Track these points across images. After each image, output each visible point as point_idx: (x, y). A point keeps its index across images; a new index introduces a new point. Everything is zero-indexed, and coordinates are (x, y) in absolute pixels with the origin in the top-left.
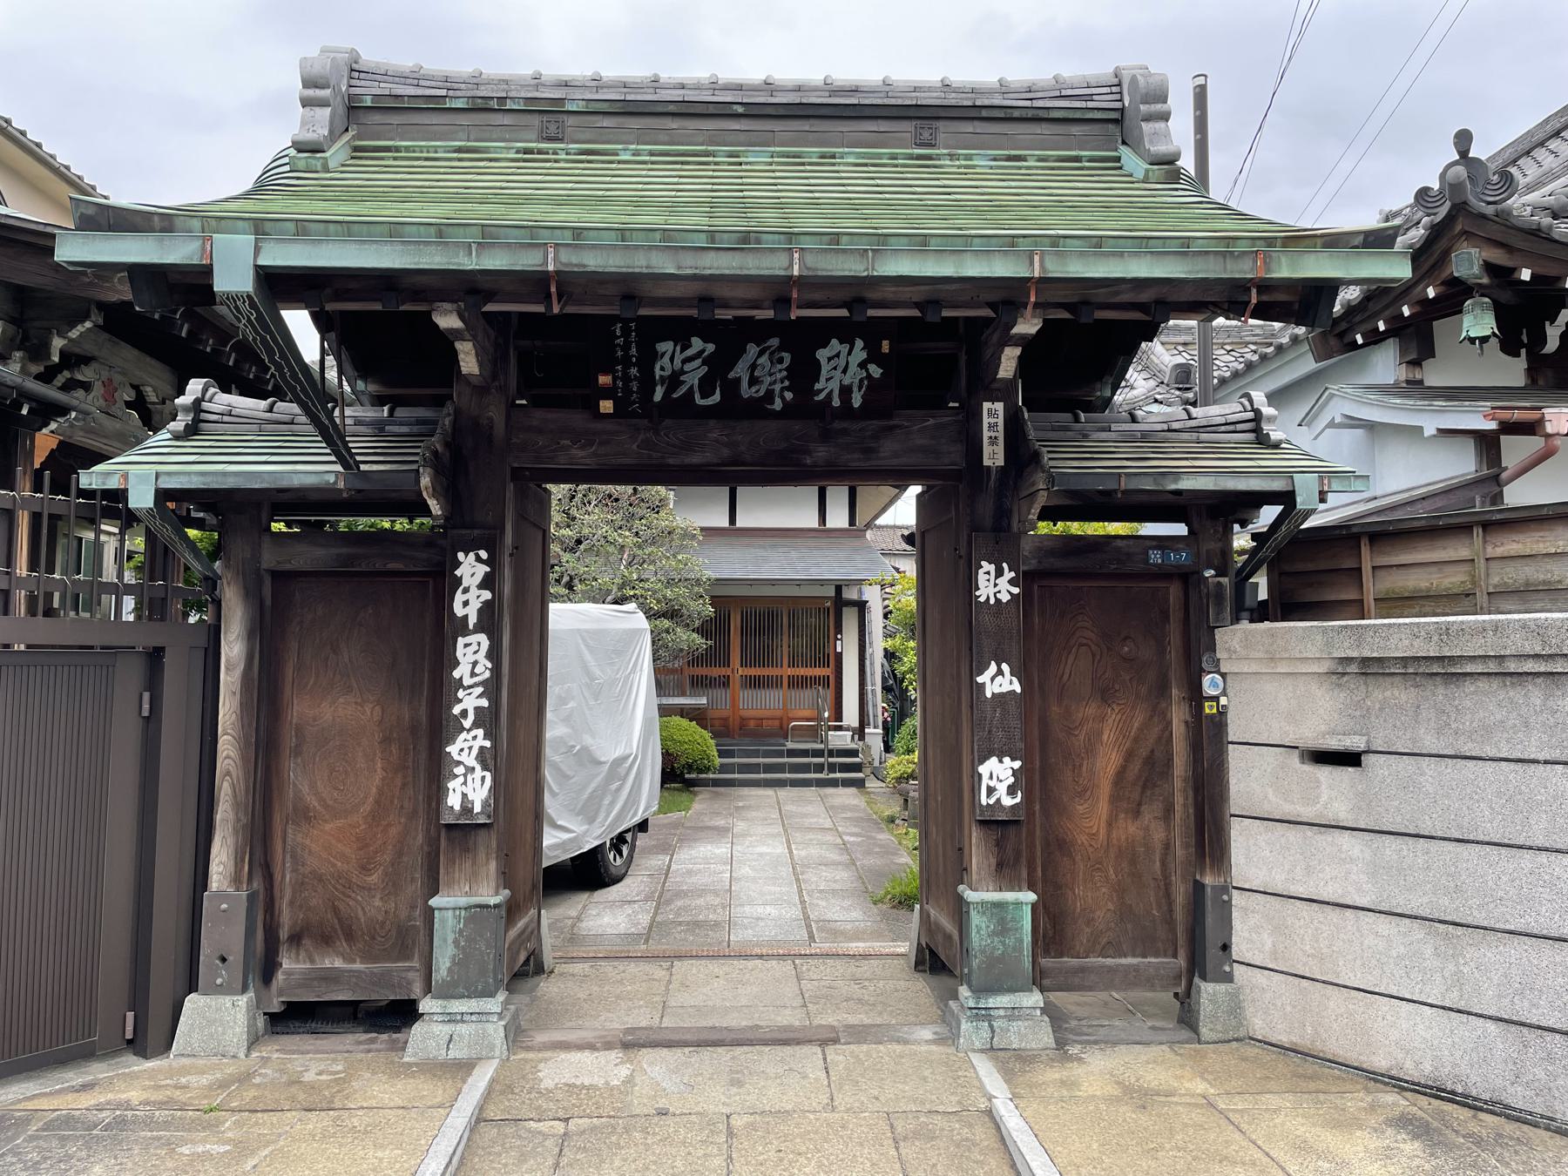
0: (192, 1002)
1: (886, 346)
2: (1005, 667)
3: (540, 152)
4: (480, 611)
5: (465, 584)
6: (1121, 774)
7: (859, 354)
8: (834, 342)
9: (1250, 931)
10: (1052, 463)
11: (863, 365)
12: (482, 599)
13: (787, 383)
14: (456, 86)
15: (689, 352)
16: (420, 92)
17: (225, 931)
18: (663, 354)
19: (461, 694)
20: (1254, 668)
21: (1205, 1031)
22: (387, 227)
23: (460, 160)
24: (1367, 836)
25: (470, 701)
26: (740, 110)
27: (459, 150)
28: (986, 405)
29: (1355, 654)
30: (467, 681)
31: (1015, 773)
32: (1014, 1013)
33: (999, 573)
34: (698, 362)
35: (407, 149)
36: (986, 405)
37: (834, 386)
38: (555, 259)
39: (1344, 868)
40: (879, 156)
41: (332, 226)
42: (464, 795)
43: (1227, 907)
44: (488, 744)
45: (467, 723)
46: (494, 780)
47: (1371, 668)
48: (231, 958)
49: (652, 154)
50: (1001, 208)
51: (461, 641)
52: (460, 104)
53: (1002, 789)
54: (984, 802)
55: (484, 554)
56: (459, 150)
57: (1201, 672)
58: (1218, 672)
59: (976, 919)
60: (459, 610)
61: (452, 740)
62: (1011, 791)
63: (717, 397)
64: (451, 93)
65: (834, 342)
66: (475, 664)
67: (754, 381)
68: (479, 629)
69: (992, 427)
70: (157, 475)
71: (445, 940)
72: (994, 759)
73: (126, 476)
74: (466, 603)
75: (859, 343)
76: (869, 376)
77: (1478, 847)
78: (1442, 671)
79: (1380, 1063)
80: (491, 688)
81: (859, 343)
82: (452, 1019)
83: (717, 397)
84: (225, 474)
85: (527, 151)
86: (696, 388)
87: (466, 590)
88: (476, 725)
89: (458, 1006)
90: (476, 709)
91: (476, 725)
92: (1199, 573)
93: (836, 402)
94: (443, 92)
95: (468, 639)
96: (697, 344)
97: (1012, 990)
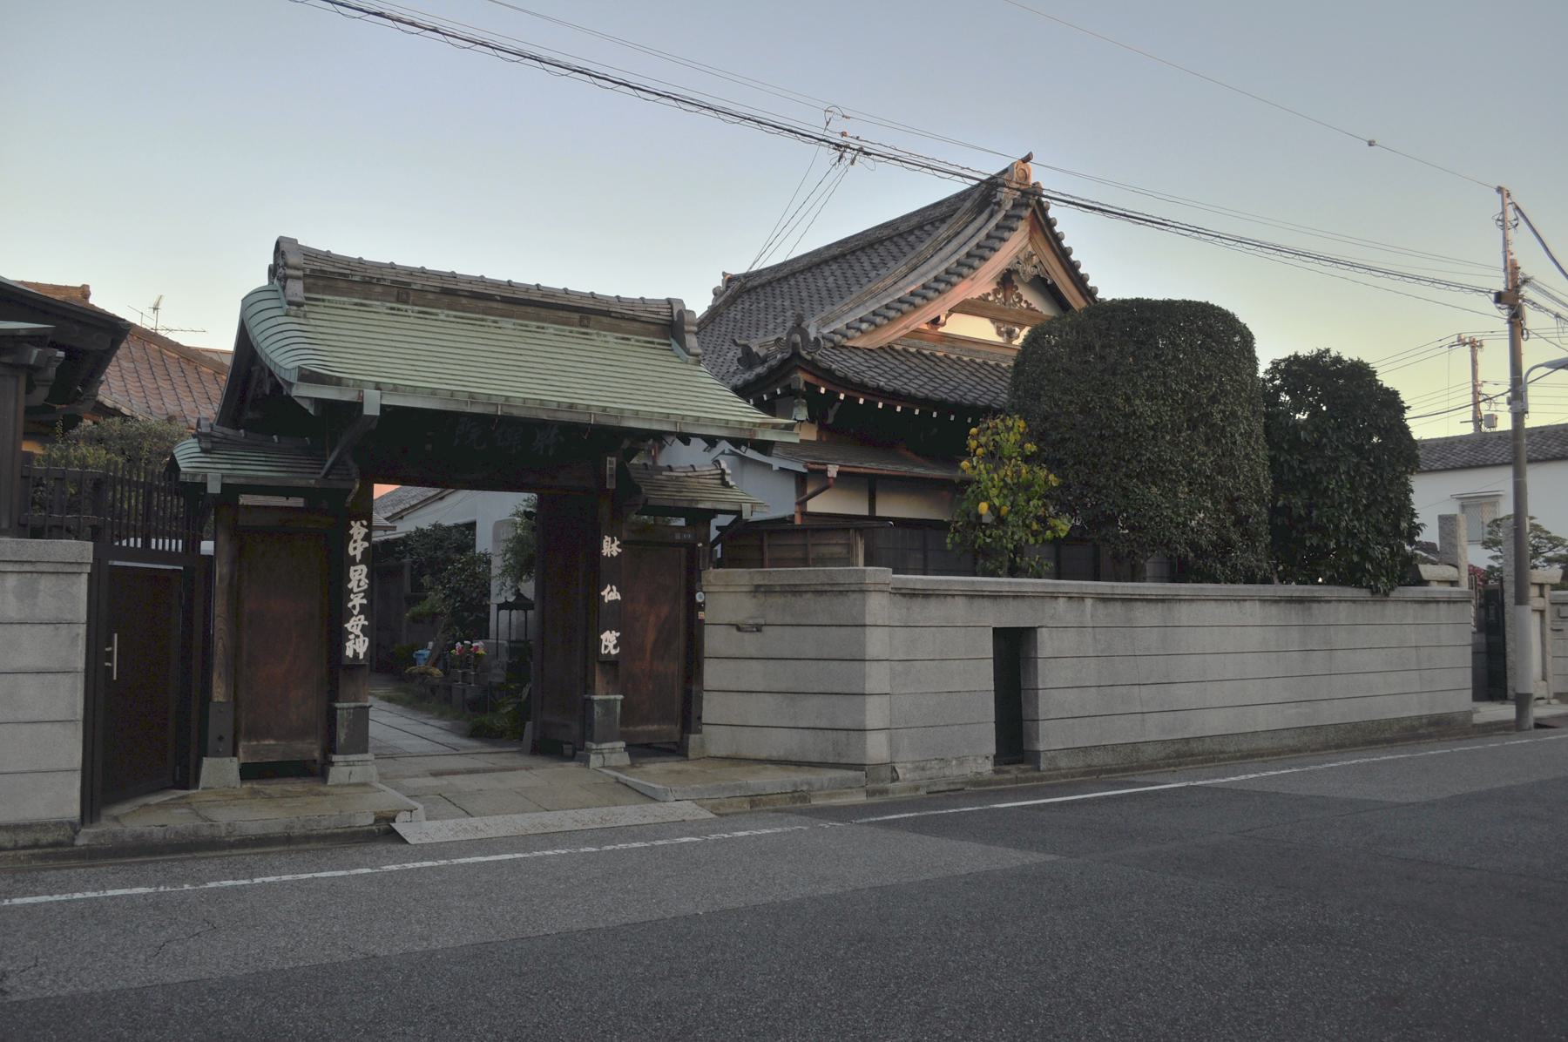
0: (206, 761)
9: (712, 708)
17: (219, 724)
21: (691, 755)
25: (357, 601)
32: (613, 750)
39: (753, 676)
43: (700, 699)
53: (611, 646)
59: (597, 709)
60: (351, 552)
62: (615, 647)
68: (361, 562)
73: (205, 476)
78: (795, 591)
79: (763, 755)
80: (368, 594)
82: (348, 764)
89: (352, 757)
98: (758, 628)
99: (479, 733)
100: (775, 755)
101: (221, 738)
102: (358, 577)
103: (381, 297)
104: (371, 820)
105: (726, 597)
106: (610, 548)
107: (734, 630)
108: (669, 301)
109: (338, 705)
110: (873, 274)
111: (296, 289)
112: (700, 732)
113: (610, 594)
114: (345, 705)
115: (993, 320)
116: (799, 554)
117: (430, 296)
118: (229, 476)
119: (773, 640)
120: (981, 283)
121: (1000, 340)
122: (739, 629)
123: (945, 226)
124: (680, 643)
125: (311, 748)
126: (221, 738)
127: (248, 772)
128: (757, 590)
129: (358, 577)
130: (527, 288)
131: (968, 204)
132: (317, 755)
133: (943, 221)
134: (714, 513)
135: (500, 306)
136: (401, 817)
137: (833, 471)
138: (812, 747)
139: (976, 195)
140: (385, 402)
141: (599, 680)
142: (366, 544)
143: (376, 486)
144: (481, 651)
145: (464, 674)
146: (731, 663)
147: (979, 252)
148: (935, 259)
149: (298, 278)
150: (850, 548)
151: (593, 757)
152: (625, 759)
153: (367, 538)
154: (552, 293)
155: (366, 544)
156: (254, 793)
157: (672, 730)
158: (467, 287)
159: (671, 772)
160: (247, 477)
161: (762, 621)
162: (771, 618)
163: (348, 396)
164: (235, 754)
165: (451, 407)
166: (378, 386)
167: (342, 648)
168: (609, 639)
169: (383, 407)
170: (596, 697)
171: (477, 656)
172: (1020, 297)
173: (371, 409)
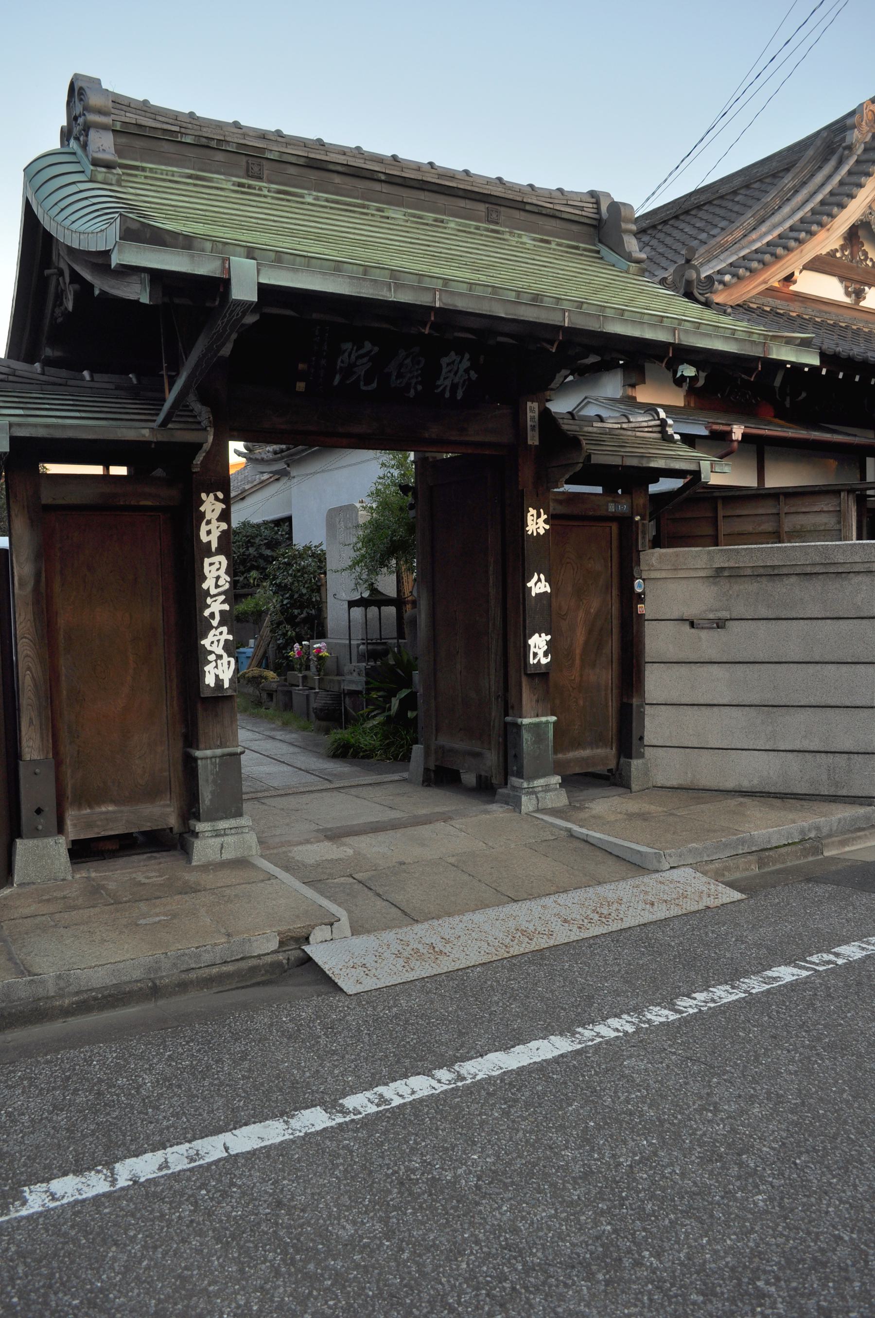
0: (20, 845)
1: (482, 359)
2: (542, 577)
3: (250, 187)
4: (219, 538)
5: (208, 517)
6: (586, 643)
7: (466, 364)
8: (453, 353)
9: (655, 726)
10: (589, 447)
11: (467, 371)
12: (221, 529)
13: (420, 379)
14: (184, 125)
15: (361, 352)
16: (159, 125)
17: (35, 790)
18: (344, 351)
19: (209, 601)
20: (663, 575)
21: (634, 787)
22: (333, 264)
23: (195, 185)
24: (727, 666)
25: (216, 606)
26: (383, 177)
27: (190, 177)
28: (529, 404)
29: (726, 565)
30: (213, 591)
31: (548, 643)
32: (547, 789)
33: (539, 516)
34: (365, 360)
35: (151, 170)
36: (529, 404)
37: (448, 383)
38: (440, 299)
39: (715, 683)
40: (469, 226)
41: (298, 258)
42: (217, 676)
43: (642, 716)
44: (231, 637)
45: (215, 623)
46: (237, 662)
47: (732, 574)
48: (46, 809)
49: (327, 200)
50: (447, 260)
51: (207, 561)
52: (189, 140)
53: (541, 653)
54: (531, 662)
55: (220, 495)
56: (190, 177)
57: (633, 579)
58: (641, 578)
59: (526, 736)
60: (204, 538)
61: (205, 636)
62: (546, 654)
63: (375, 385)
64: (183, 130)
65: (453, 353)
66: (218, 578)
67: (400, 376)
68: (219, 551)
69: (532, 418)
70: (11, 425)
71: (207, 780)
72: (537, 635)
74: (209, 532)
75: (467, 356)
76: (469, 379)
77: (787, 665)
78: (774, 574)
79: (730, 785)
81: (467, 356)
82: (217, 834)
83: (375, 385)
84: (64, 426)
85: (240, 185)
86: (362, 378)
87: (209, 522)
88: (221, 624)
89: (222, 825)
90: (221, 612)
91: (221, 624)
92: (632, 518)
93: (447, 395)
94: (177, 129)
95: (212, 560)
96: (368, 346)
97: (544, 776)
98: (720, 624)
99: (343, 752)
100: (746, 785)
101: (39, 811)
102: (215, 573)
103: (226, 170)
104: (274, 945)
105: (674, 584)
106: (536, 524)
107: (686, 627)
108: (593, 194)
109: (198, 754)
110: (703, 236)
111: (103, 144)
112: (642, 756)
113: (538, 586)
114: (209, 753)
115: (842, 279)
116: (768, 527)
117: (292, 170)
118: (19, 425)
119: (740, 639)
120: (829, 240)
121: (847, 300)
122: (692, 624)
123: (790, 176)
124: (612, 646)
125: (164, 813)
126: (39, 811)
127: (82, 852)
128: (718, 574)
129: (215, 573)
130: (418, 167)
131: (810, 152)
132: (173, 821)
133: (788, 170)
134: (656, 474)
135: (385, 188)
136: (319, 934)
137: (738, 432)
138: (797, 774)
139: (818, 142)
140: (263, 281)
141: (528, 698)
142: (224, 526)
143: (230, 443)
144: (324, 653)
145: (305, 678)
146: (684, 670)
147: (833, 199)
148: (786, 210)
149: (104, 127)
150: (840, 515)
151: (524, 799)
152: (559, 799)
153: (225, 516)
154: (451, 175)
155: (224, 526)
156: (94, 891)
157: (603, 755)
158: (342, 159)
159: (631, 816)
160: (47, 426)
161: (725, 614)
162: (740, 610)
163: (206, 268)
164: (61, 829)
165: (366, 291)
166: (250, 253)
167: (200, 675)
168: (538, 643)
169: (263, 289)
170: (526, 721)
171: (320, 659)
172: (865, 254)
173: (244, 291)
